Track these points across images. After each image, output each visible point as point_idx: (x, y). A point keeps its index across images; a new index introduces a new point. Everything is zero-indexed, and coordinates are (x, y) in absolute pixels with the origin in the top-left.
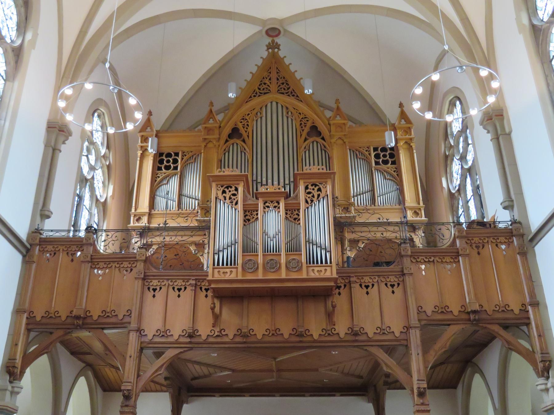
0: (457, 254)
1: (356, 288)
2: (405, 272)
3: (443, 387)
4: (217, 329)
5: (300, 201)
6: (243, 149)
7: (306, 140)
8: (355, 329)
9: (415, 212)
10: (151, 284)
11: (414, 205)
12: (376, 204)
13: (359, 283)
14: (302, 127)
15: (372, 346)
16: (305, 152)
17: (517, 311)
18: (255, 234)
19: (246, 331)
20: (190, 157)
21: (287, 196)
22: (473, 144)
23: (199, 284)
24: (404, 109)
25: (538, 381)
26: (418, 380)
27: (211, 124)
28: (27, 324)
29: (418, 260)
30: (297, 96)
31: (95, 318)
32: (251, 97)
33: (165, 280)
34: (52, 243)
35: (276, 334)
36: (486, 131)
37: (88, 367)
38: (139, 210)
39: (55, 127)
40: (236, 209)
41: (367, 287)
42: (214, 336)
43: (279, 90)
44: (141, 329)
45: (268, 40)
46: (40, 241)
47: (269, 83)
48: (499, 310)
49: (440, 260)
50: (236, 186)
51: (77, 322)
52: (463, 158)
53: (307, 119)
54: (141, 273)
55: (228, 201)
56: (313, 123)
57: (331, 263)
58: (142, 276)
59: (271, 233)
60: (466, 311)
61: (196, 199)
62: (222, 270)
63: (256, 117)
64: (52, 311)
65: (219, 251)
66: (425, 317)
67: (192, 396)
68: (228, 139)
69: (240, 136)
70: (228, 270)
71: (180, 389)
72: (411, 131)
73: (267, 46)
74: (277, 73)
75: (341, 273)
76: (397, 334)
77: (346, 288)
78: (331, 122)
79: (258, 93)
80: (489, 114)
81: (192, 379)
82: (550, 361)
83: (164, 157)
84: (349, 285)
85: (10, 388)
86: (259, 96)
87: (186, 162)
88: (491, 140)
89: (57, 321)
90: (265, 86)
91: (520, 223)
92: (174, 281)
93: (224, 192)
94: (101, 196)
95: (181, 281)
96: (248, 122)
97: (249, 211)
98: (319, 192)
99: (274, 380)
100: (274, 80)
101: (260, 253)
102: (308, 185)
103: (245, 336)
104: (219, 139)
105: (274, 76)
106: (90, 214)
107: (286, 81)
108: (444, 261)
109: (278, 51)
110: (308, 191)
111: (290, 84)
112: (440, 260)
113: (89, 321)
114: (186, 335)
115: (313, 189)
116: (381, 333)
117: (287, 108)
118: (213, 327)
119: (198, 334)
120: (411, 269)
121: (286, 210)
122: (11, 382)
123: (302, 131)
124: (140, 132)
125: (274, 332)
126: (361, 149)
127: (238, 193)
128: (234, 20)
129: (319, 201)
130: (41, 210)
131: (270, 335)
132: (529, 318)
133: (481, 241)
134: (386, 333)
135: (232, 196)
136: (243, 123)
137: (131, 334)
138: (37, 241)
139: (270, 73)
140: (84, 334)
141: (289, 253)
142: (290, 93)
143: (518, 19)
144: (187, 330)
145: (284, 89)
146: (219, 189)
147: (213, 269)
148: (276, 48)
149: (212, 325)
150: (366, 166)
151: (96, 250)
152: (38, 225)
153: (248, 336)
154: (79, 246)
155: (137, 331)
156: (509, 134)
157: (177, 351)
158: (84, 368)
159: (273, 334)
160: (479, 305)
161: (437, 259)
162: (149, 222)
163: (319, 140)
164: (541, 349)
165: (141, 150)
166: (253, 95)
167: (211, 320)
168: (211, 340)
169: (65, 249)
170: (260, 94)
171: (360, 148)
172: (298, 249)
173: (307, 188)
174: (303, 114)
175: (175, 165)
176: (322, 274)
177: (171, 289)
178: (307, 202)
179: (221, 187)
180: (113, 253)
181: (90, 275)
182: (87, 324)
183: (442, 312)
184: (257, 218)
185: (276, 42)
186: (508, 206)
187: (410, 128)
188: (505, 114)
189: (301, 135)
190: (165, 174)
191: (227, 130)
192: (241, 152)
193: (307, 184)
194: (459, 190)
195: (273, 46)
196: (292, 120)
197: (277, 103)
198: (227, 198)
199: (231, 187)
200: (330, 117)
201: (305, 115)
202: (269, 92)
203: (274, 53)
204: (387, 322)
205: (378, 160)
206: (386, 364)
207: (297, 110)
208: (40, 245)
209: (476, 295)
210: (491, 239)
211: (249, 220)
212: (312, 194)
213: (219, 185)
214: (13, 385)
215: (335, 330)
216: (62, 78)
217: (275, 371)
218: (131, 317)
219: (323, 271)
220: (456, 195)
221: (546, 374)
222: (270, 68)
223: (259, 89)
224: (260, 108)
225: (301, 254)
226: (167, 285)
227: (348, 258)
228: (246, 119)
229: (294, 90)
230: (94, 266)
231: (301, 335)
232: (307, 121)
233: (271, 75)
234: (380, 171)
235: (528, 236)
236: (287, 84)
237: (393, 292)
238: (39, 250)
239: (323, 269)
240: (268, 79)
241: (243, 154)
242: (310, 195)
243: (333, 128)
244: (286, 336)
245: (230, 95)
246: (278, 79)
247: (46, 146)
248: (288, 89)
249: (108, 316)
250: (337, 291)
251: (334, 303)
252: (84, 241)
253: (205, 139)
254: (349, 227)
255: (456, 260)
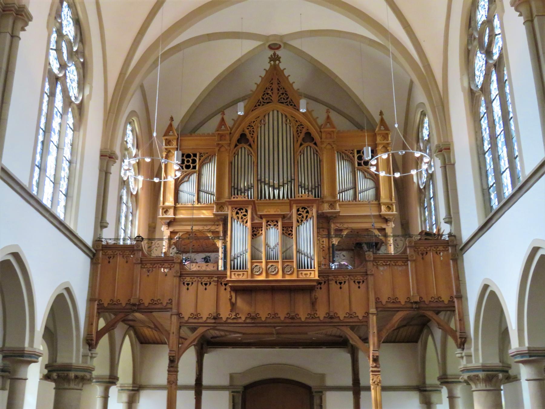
0: (407, 260)
1: (333, 284)
2: (369, 273)
3: (408, 342)
4: (234, 314)
5: (293, 221)
6: (250, 153)
7: (301, 145)
8: (331, 314)
9: (388, 207)
10: (185, 280)
11: (388, 201)
12: (357, 200)
13: (335, 281)
14: (298, 134)
15: (343, 326)
16: (300, 156)
17: (446, 302)
18: (260, 246)
19: (254, 315)
20: (206, 158)
21: (284, 217)
22: (503, 33)
23: (220, 280)
24: (384, 117)
25: (457, 351)
26: (373, 351)
27: (223, 130)
28: (98, 309)
29: (379, 264)
30: (295, 106)
31: (146, 304)
32: (256, 106)
33: (195, 277)
34: (111, 249)
35: (275, 317)
36: (518, 13)
37: (131, 328)
38: (167, 204)
39: (106, 156)
40: (246, 227)
41: (340, 283)
42: (232, 318)
43: (279, 100)
44: (179, 313)
45: (271, 53)
46: (102, 247)
47: (271, 93)
48: (434, 300)
49: (394, 264)
50: (246, 208)
51: (134, 308)
52: (489, 53)
53: (302, 126)
54: (178, 273)
55: (240, 220)
56: (308, 130)
57: (314, 268)
58: (179, 275)
59: (272, 244)
60: (410, 302)
61: (211, 194)
62: (237, 273)
63: (260, 124)
64: (115, 300)
65: (235, 258)
66: (381, 306)
67: (210, 348)
68: (238, 144)
69: (247, 141)
70: (241, 273)
71: (202, 344)
72: (388, 137)
73: (269, 58)
74: (278, 84)
75: (321, 273)
76: (361, 318)
77: (325, 285)
78: (322, 130)
79: (262, 102)
80: (440, 147)
81: (212, 338)
82: (465, 338)
83: (185, 158)
84: (327, 282)
85: (90, 354)
86: (263, 105)
87: (202, 162)
88: (441, 167)
89: (119, 307)
90: (267, 96)
91: (455, 236)
92: (202, 278)
93: (237, 213)
94: (133, 189)
95: (207, 278)
96: (253, 128)
97: (256, 228)
98: (307, 214)
99: (275, 338)
100: (275, 91)
101: (264, 261)
102: (299, 208)
103: (253, 318)
104: (230, 144)
105: (275, 86)
106: (127, 207)
107: (286, 91)
108: (397, 264)
109: (279, 63)
110: (299, 213)
111: (289, 95)
112: (394, 264)
113: (142, 307)
114: (212, 318)
115: (303, 212)
116: (349, 317)
117: (286, 116)
118: (231, 312)
119: (221, 316)
120: (372, 271)
121: (283, 227)
122: (90, 350)
123: (298, 137)
124: (164, 136)
125: (273, 316)
126: (347, 152)
127: (247, 214)
128: (242, 38)
129: (307, 221)
130: (101, 223)
131: (271, 318)
132: (454, 307)
133: (425, 250)
134: (353, 317)
135: (243, 217)
136: (249, 130)
137: (173, 317)
138: (101, 248)
139: (272, 84)
140: (138, 315)
141: (284, 261)
142: (288, 103)
143: (462, 80)
144: (212, 313)
145: (284, 99)
146: (234, 210)
147: (231, 272)
148: (277, 60)
149: (230, 310)
150: (349, 168)
151: (144, 254)
152: (100, 234)
153: (255, 318)
154: (132, 251)
155: (177, 314)
156: (454, 164)
157: (205, 329)
158: (128, 328)
159: (273, 317)
160: (420, 298)
161: (392, 263)
162: (175, 214)
163: (312, 144)
164: (461, 330)
165: (166, 152)
166: (258, 104)
167: (229, 307)
168: (229, 321)
169: (121, 253)
170: (264, 104)
171: (346, 150)
172: (291, 258)
173: (298, 210)
174: (299, 121)
175: (194, 165)
176: (308, 276)
177: (200, 284)
178: (298, 221)
179: (235, 210)
180: (157, 257)
181: (140, 274)
182: (141, 309)
183: (393, 302)
184: (262, 233)
185: (277, 54)
186: (449, 221)
187: (387, 134)
188: (451, 148)
189: (297, 141)
190: (186, 172)
191: (236, 136)
192: (248, 155)
193: (298, 208)
194: (424, 188)
195: (275, 58)
196: (290, 127)
197: (278, 111)
198: (240, 218)
199: (242, 209)
200: (322, 125)
201: (301, 123)
202: (271, 101)
203: (275, 65)
204: (354, 310)
205: (360, 162)
206: (352, 339)
207: (294, 118)
208: (102, 250)
209: (418, 289)
210: (433, 248)
211: (256, 235)
212: (302, 216)
213: (234, 207)
214: (92, 352)
215: (317, 315)
216: (109, 113)
217: (275, 334)
218: (172, 304)
219: (309, 274)
220: (423, 190)
221: (462, 346)
222: (272, 79)
223: (263, 99)
224: (263, 116)
225: (293, 262)
226: (197, 281)
227: (333, 245)
228: (252, 126)
229: (292, 100)
230: (143, 267)
231: (293, 318)
232: (303, 128)
233: (273, 86)
234: (361, 171)
235: (460, 246)
236: (286, 94)
237: (359, 287)
238: (102, 254)
239: (308, 272)
240: (270, 89)
241: (250, 156)
242: (300, 216)
243: (324, 135)
244: (282, 318)
245: (239, 113)
246: (278, 90)
247: (101, 170)
248: (287, 98)
249: (156, 304)
250: (319, 286)
251: (316, 297)
252: (135, 248)
253: (218, 144)
254: (334, 222)
255: (406, 264)
